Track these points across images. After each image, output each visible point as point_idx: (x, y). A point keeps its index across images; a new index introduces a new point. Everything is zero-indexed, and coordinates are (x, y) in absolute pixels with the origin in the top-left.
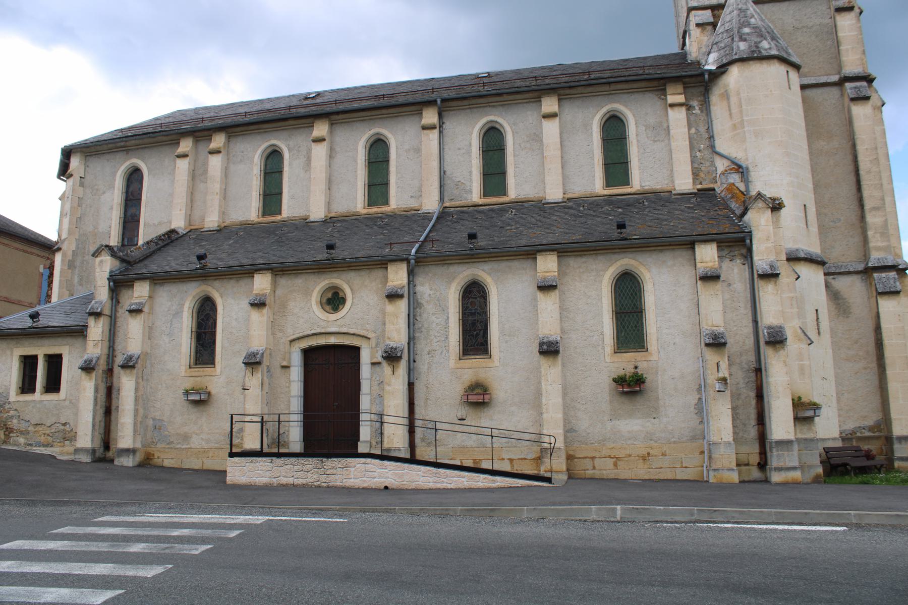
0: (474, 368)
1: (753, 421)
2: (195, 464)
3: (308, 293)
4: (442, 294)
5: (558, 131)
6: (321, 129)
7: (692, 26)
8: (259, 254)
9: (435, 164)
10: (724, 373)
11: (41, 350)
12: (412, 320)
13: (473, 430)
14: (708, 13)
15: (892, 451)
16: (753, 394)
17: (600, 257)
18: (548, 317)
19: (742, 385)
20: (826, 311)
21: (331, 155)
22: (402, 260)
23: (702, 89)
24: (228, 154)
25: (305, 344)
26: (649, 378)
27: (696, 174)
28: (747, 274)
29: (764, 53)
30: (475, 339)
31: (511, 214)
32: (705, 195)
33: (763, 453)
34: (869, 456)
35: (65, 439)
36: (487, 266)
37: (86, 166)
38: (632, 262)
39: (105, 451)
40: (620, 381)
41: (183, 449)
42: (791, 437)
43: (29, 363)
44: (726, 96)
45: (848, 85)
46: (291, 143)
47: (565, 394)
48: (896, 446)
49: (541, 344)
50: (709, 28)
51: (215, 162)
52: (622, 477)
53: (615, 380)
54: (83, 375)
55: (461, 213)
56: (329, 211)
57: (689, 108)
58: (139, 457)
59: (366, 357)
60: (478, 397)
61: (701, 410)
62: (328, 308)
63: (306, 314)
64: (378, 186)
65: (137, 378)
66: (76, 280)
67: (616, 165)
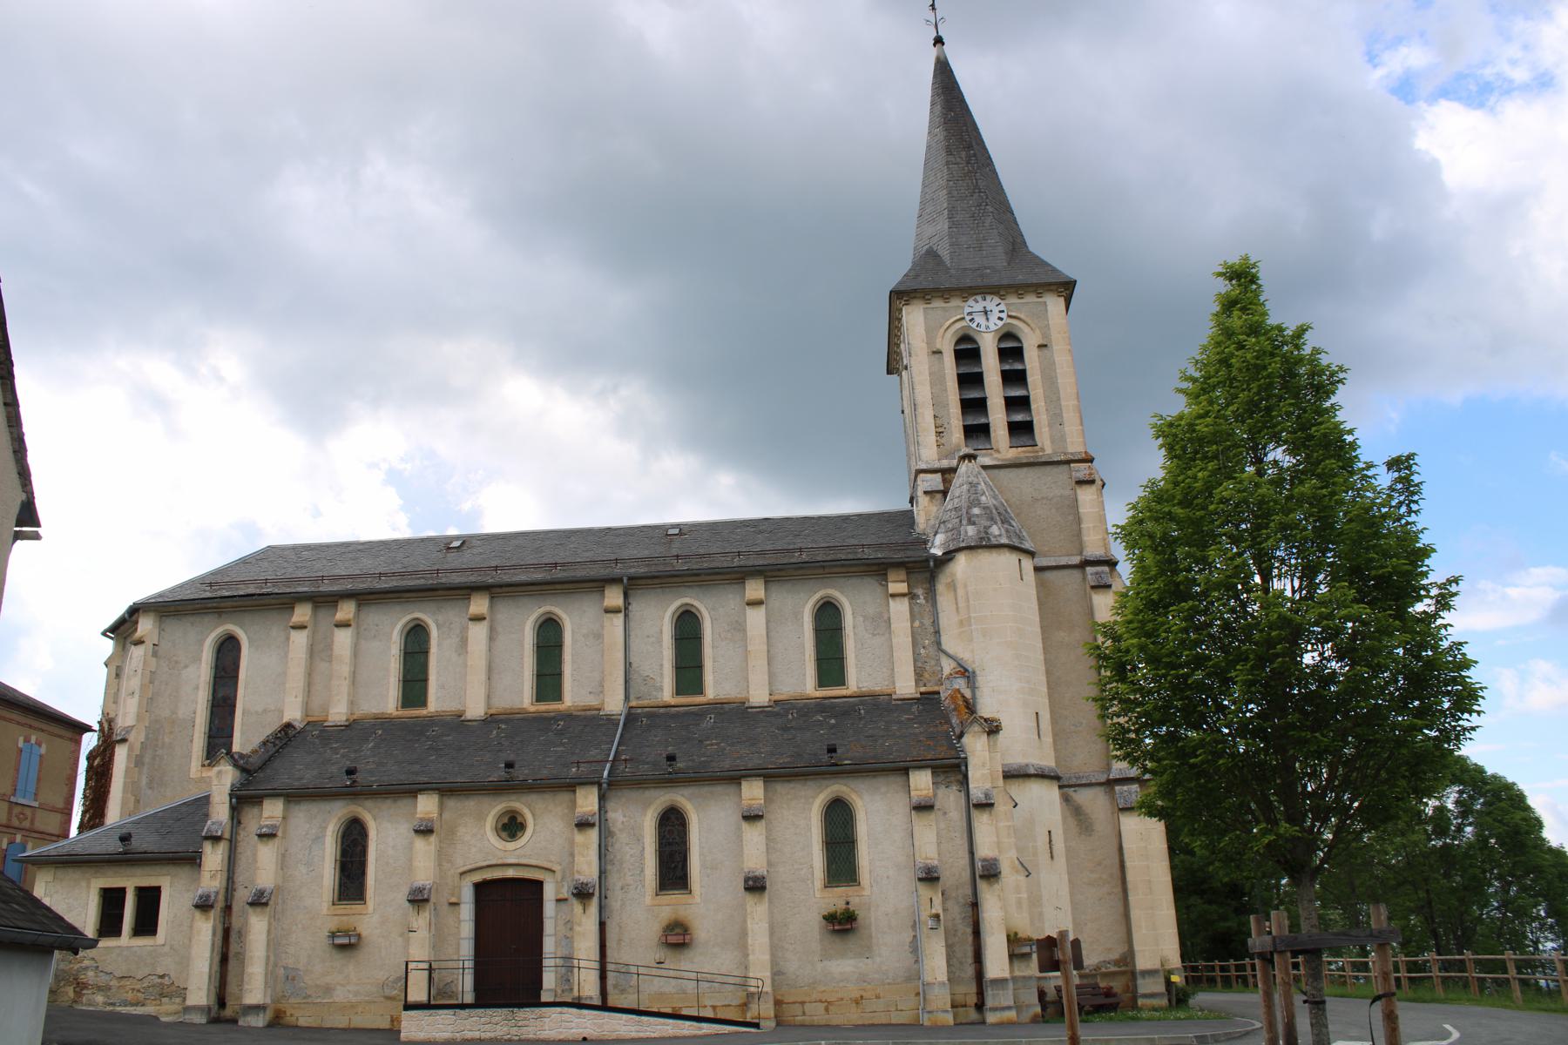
0: (673, 905)
1: (970, 960)
2: (340, 1021)
3: (481, 818)
4: (637, 824)
5: (764, 621)
6: (479, 605)
7: (920, 493)
8: (417, 767)
9: (621, 655)
10: (938, 909)
11: (130, 881)
13: (672, 973)
14: (938, 476)
15: (1135, 986)
16: (969, 930)
17: (810, 783)
18: (754, 849)
19: (958, 921)
20: (1061, 832)
21: (492, 638)
22: (592, 783)
23: (928, 575)
24: (358, 627)
25: (478, 877)
26: (861, 914)
27: (919, 675)
28: (963, 802)
29: (994, 541)
30: (673, 871)
31: (710, 720)
32: (929, 700)
33: (981, 993)
34: (1109, 993)
35: (162, 995)
36: (687, 791)
37: (161, 630)
38: (844, 788)
39: (222, 1009)
40: (830, 918)
41: (324, 1004)
42: (1006, 975)
43: (112, 900)
44: (952, 586)
45: (1089, 570)
46: (440, 618)
47: (772, 934)
48: (1140, 981)
49: (747, 880)
50: (939, 496)
51: (343, 638)
52: (835, 1022)
53: (825, 917)
54: (198, 914)
55: (650, 716)
56: (489, 706)
57: (911, 595)
58: (269, 1015)
59: (549, 893)
60: (677, 937)
61: (915, 948)
62: (504, 834)
63: (479, 843)
64: (549, 679)
66: (144, 781)
67: (830, 664)
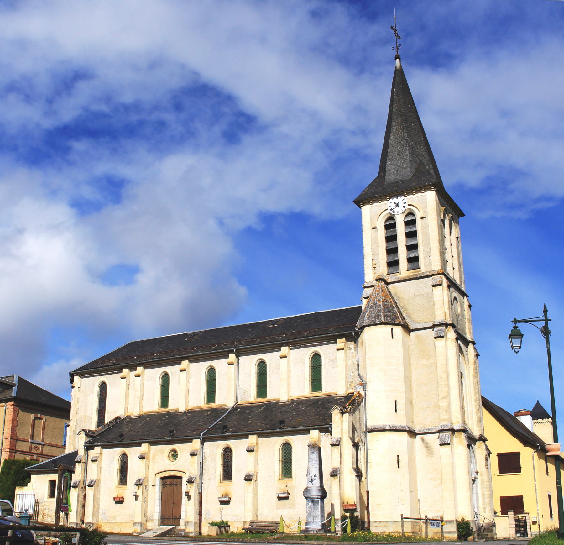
12: (201, 465)
30: (227, 474)
37: (81, 381)
65: (95, 490)
